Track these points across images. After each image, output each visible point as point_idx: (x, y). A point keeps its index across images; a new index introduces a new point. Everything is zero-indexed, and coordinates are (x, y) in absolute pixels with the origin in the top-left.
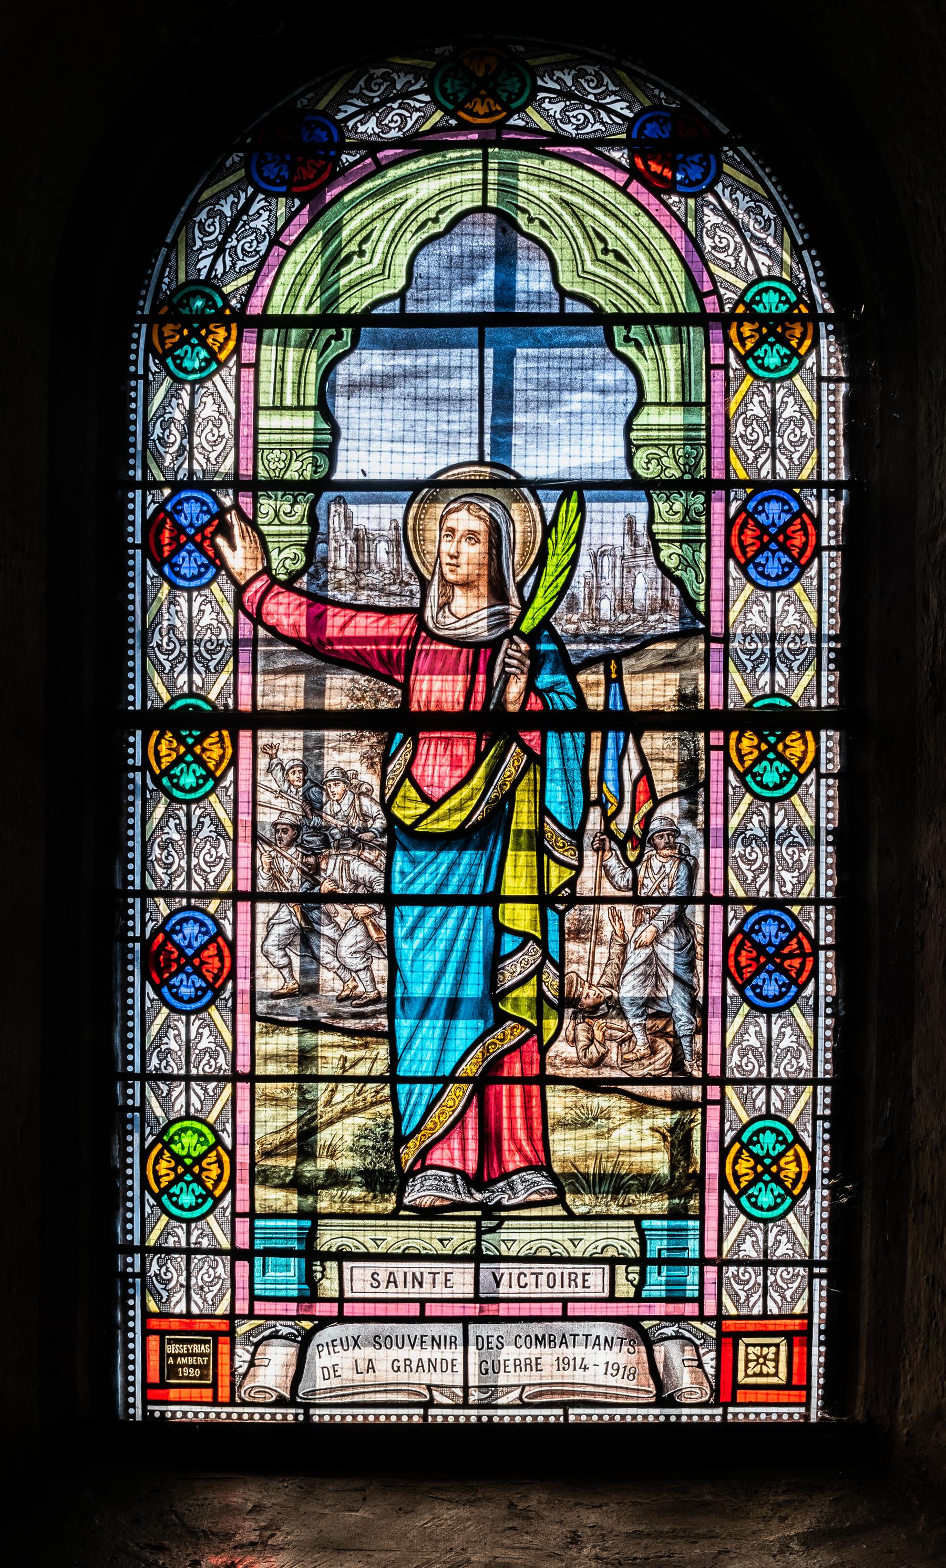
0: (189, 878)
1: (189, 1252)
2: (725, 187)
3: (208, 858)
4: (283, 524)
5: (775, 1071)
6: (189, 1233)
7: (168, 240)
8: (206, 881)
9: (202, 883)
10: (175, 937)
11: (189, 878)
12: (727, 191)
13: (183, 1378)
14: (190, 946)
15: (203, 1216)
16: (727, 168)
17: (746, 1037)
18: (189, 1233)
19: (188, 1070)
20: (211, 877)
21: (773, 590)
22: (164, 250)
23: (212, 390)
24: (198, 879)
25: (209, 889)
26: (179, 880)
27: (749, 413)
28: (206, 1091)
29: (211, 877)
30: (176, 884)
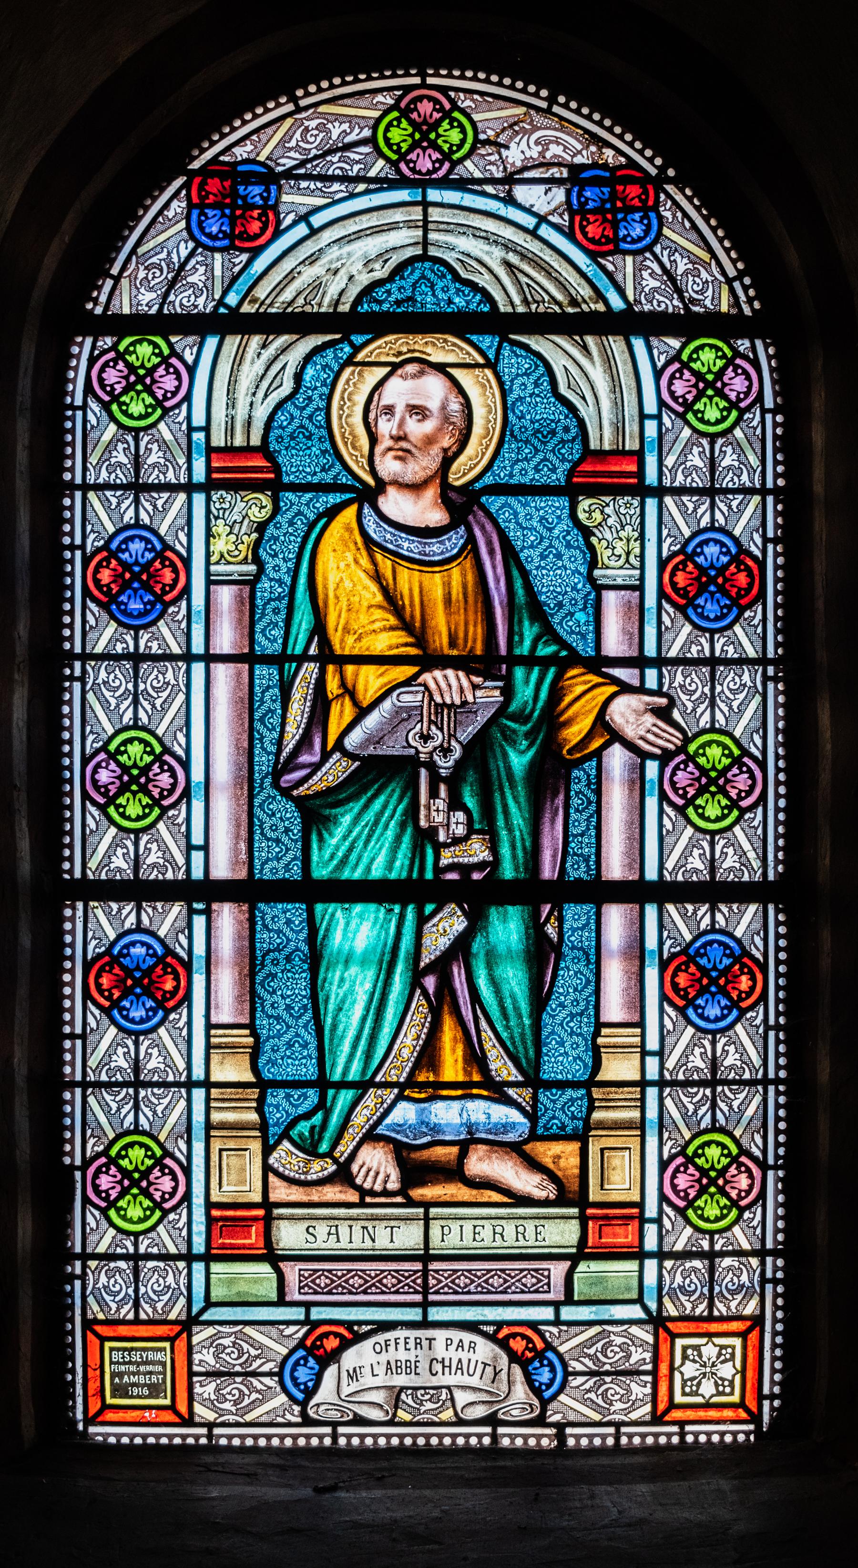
0: (137, 1305)
1: (136, 1258)
2: (663, 248)
3: (155, 683)
4: (229, 563)
5: (708, 1092)
6: (136, 639)
7: (115, 271)
8: (155, 1309)
9: (150, 1311)
10: (121, 1162)
11: (137, 1305)
12: (666, 253)
13: (132, 1397)
14: (135, 1197)
15: (153, 1228)
16: (666, 231)
17: (644, 283)
18: (136, 639)
19: (137, 1093)
20: (159, 1306)
21: (712, 632)
22: (109, 283)
23: (157, 436)
24: (146, 1307)
25: (157, 1317)
26: (127, 1308)
27: (689, 464)
28: (731, 909)
29: (159, 1306)
30: (123, 1312)
